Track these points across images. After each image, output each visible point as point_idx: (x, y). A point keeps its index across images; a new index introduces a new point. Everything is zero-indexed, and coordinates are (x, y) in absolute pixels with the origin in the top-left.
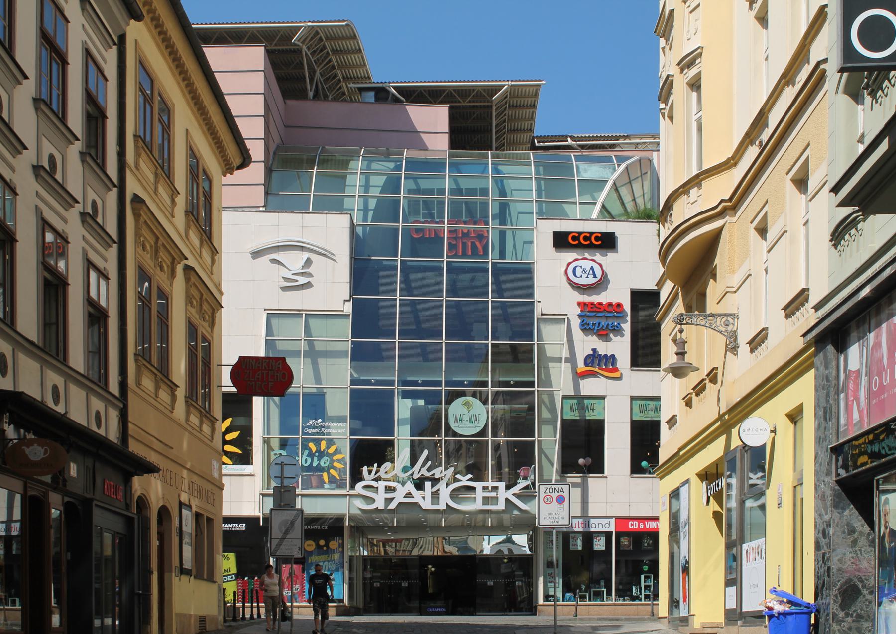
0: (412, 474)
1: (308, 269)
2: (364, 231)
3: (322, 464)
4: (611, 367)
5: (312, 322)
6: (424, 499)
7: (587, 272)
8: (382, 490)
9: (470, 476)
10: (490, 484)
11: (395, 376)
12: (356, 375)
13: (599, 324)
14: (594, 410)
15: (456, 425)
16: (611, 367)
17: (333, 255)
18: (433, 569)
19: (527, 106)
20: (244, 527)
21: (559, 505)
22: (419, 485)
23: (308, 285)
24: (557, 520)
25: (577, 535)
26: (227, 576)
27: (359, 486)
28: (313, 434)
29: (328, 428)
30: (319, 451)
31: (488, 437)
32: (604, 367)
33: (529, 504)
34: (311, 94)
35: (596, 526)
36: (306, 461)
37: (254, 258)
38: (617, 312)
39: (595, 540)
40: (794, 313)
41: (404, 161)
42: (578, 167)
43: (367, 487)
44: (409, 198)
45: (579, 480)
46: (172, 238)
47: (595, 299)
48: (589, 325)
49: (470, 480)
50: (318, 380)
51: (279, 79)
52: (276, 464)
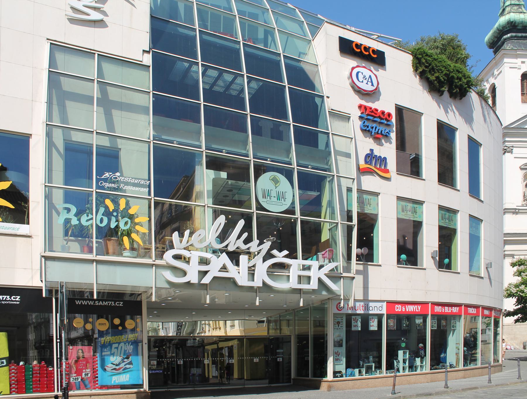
4: (383, 168)
7: (367, 79)
8: (194, 261)
9: (286, 252)
15: (264, 200)
20: (17, 299)
23: (99, 24)
25: (357, 317)
27: (168, 255)
28: (110, 189)
35: (377, 309)
36: (102, 221)
40: (378, 193)
43: (177, 257)
49: (286, 256)
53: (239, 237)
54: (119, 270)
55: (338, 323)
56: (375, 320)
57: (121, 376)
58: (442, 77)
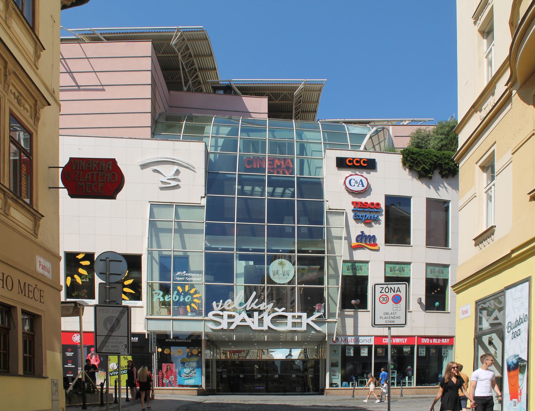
0: (246, 307)
1: (178, 176)
2: (215, 157)
3: (186, 300)
4: (372, 243)
5: (180, 210)
6: (253, 323)
7: (358, 183)
8: (225, 317)
9: (283, 309)
10: (297, 314)
11: (234, 246)
12: (208, 245)
13: (366, 216)
14: (361, 270)
15: (275, 277)
16: (372, 243)
17: (194, 167)
18: (257, 367)
19: (311, 111)
20: (137, 339)
21: (395, 305)
22: (250, 315)
23: (177, 187)
24: (393, 320)
25: (350, 347)
26: (123, 370)
27: (210, 314)
29: (191, 277)
30: (184, 291)
31: (295, 285)
32: (368, 243)
33: (322, 327)
34: (185, 89)
35: (363, 341)
36: (175, 298)
37: (142, 169)
38: (377, 209)
39: (362, 350)
41: (241, 121)
42: (347, 128)
44: (244, 139)
45: (352, 313)
46: (42, 92)
47: (363, 200)
48: (359, 216)
50: (184, 246)
51: (163, 69)
52: (101, 260)
53: (252, 302)
54: (184, 323)
55: (335, 351)
56: (366, 349)
57: (190, 380)
58: (427, 167)
